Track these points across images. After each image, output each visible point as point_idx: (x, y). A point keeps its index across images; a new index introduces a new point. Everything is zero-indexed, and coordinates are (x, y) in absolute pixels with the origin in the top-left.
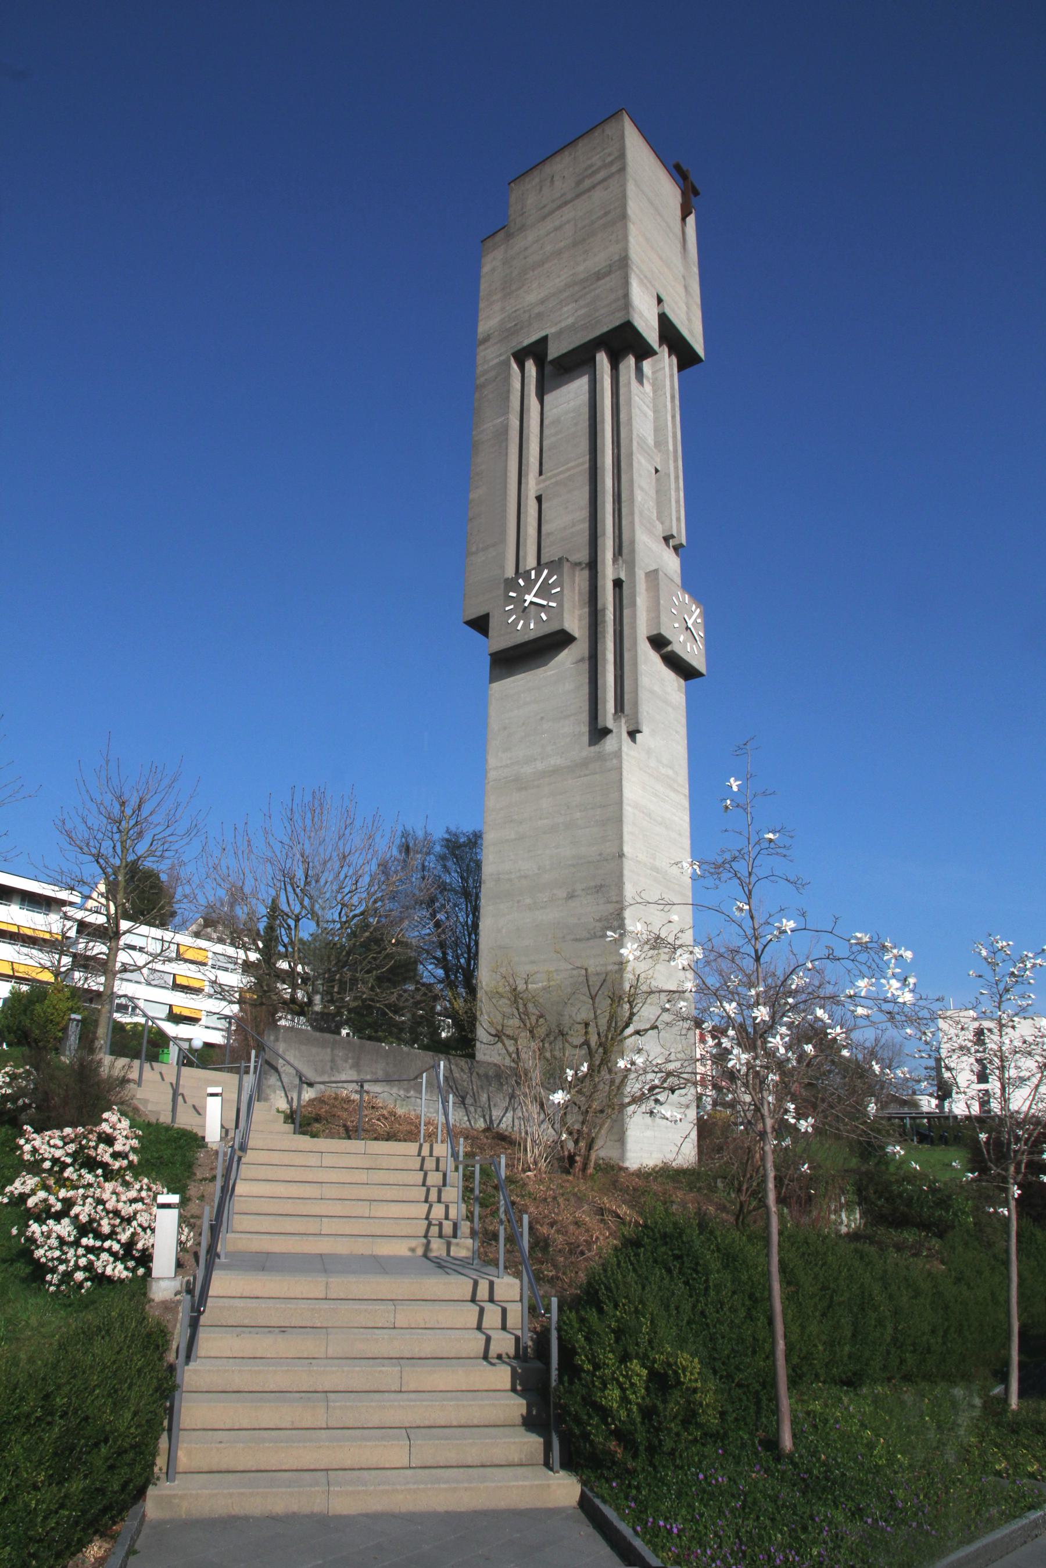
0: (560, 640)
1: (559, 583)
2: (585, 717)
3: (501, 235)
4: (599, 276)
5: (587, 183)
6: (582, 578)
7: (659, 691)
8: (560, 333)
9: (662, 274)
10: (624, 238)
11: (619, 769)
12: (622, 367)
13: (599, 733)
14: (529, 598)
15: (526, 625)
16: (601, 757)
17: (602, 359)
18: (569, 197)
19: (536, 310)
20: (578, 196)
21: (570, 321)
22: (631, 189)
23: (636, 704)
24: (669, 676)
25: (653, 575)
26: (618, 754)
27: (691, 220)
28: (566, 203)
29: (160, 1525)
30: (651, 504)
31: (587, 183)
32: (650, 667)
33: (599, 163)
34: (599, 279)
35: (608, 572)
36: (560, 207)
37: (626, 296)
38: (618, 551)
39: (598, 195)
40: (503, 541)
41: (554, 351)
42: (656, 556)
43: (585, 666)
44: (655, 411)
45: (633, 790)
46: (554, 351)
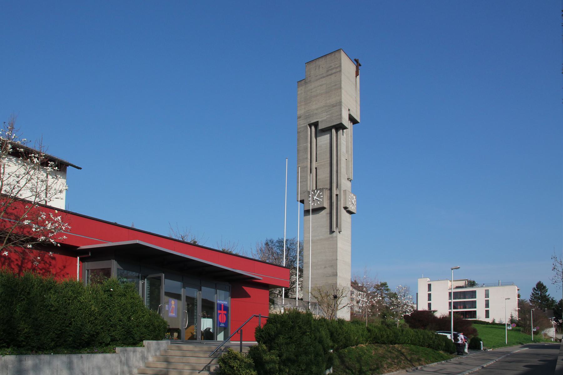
0: (323, 208)
1: (322, 195)
2: (329, 227)
3: (303, 82)
4: (334, 106)
5: (330, 72)
6: (327, 193)
7: (345, 217)
8: (322, 121)
9: (350, 102)
10: (340, 95)
11: (337, 240)
12: (339, 133)
13: (332, 232)
14: (315, 197)
15: (314, 204)
16: (332, 237)
17: (334, 131)
18: (324, 75)
19: (315, 112)
20: (327, 76)
21: (325, 118)
22: (343, 77)
23: (341, 225)
24: (348, 214)
25: (345, 191)
26: (336, 237)
27: (358, 77)
28: (324, 77)
29: (66, 208)
30: (345, 170)
31: (330, 72)
32: (344, 213)
33: (333, 66)
34: (333, 107)
35: (335, 192)
36: (321, 78)
37: (341, 115)
38: (337, 187)
39: (333, 77)
40: (307, 180)
41: (321, 127)
42: (346, 185)
43: (329, 215)
44: (346, 142)
45: (339, 245)
46: (321, 127)
